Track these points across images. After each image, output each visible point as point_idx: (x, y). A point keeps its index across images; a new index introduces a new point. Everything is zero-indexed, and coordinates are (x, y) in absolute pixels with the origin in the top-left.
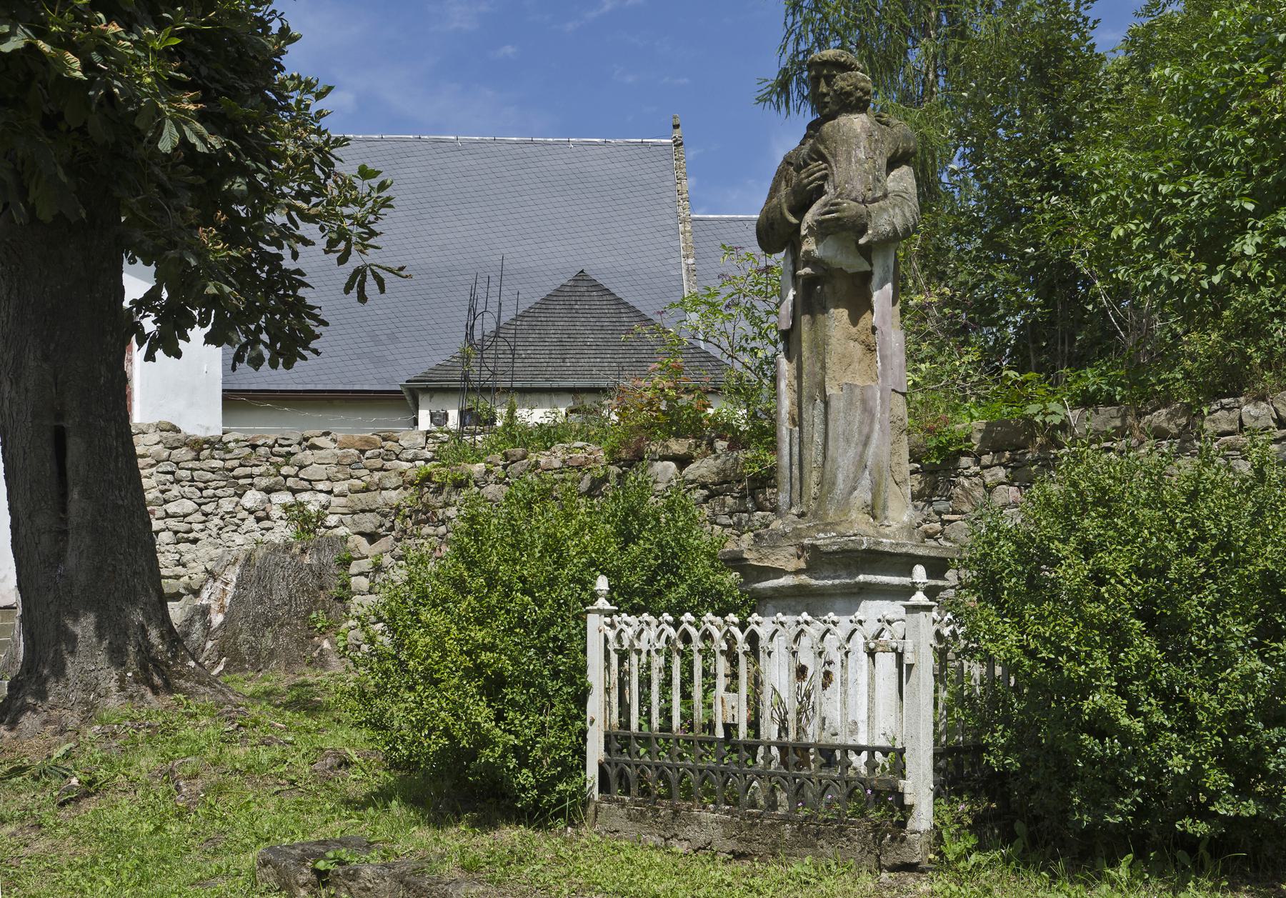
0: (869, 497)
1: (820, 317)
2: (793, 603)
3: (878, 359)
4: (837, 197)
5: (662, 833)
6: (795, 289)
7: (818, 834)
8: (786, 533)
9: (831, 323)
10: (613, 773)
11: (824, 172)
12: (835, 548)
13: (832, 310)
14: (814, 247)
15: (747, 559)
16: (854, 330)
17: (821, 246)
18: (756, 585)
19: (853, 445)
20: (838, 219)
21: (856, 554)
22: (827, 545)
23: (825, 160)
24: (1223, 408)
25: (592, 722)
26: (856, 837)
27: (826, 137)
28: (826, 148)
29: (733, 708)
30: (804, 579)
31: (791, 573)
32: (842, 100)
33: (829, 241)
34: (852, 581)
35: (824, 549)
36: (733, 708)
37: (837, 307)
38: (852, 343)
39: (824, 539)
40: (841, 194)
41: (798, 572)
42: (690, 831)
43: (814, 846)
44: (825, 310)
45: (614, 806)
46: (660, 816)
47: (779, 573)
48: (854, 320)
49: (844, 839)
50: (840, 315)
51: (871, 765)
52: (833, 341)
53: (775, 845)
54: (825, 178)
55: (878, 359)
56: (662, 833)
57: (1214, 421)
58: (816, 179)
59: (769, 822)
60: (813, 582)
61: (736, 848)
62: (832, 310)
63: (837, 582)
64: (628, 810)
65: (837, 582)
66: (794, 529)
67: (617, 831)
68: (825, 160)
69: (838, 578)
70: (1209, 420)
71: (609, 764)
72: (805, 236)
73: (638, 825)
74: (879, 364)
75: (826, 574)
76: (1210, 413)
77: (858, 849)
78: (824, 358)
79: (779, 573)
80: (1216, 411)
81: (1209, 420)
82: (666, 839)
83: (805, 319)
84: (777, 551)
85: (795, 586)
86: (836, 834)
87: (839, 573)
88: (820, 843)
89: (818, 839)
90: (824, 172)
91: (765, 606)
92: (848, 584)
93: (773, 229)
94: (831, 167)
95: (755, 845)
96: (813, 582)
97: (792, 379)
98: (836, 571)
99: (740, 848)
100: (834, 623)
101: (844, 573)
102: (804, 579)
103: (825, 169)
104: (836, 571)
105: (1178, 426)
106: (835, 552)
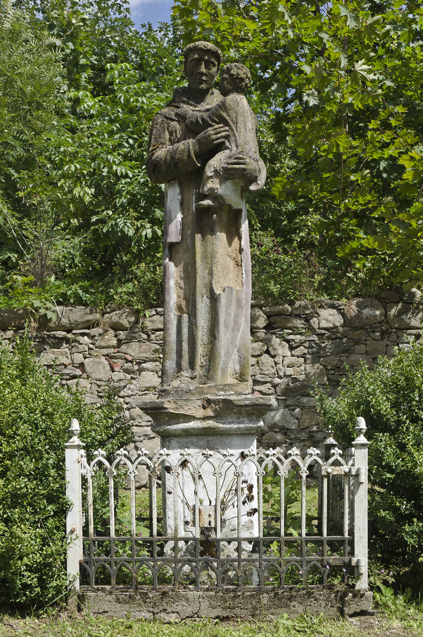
0: (238, 367)
1: (209, 237)
2: (195, 440)
3: (243, 272)
4: (239, 153)
5: (151, 609)
6: (183, 214)
7: (290, 599)
8: (190, 390)
9: (217, 242)
10: (92, 571)
11: (227, 133)
12: (247, 402)
13: (218, 233)
14: (218, 186)
15: (166, 408)
16: (230, 249)
17: (224, 186)
18: (169, 427)
19: (230, 330)
20: (244, 169)
21: (263, 407)
22: (240, 400)
23: (226, 124)
24: (157, 313)
25: (72, 532)
26: (321, 598)
27: (229, 107)
28: (229, 116)
29: (210, 516)
30: (211, 423)
31: (199, 419)
32: (235, 83)
33: (229, 183)
34: (255, 426)
35: (238, 403)
36: (210, 516)
37: (221, 232)
38: (229, 259)
39: (224, 395)
40: (242, 152)
41: (205, 418)
42: (179, 606)
43: (287, 606)
44: (213, 232)
45: (100, 593)
46: (149, 598)
47: (188, 418)
48: (230, 242)
49: (313, 599)
50: (222, 236)
51: (238, 550)
52: (219, 255)
53: (255, 608)
54: (227, 137)
55: (243, 272)
56: (151, 609)
57: (152, 322)
58: (222, 137)
59: (249, 593)
60: (221, 425)
61: (221, 614)
62: (218, 233)
63: (242, 426)
64: (116, 596)
65: (242, 426)
66: (197, 388)
67: (107, 612)
68: (226, 124)
69: (242, 422)
70: (150, 321)
71: (87, 562)
72: (211, 177)
73: (127, 605)
74: (244, 276)
75: (230, 420)
76: (150, 317)
77: (323, 605)
78: (211, 267)
79: (188, 418)
80: (154, 315)
81: (150, 321)
82: (154, 614)
83: (198, 237)
84: (189, 403)
85: (204, 428)
86: (306, 597)
87: (241, 420)
88: (292, 604)
89: (291, 602)
90: (227, 133)
91: (169, 442)
92: (251, 427)
93: (176, 166)
94: (233, 130)
95: (237, 611)
96: (221, 425)
97: (178, 279)
98: (238, 418)
99: (225, 614)
100: (168, 455)
101: (245, 420)
102: (211, 423)
103: (228, 131)
104: (238, 418)
105: (130, 323)
106: (246, 406)
